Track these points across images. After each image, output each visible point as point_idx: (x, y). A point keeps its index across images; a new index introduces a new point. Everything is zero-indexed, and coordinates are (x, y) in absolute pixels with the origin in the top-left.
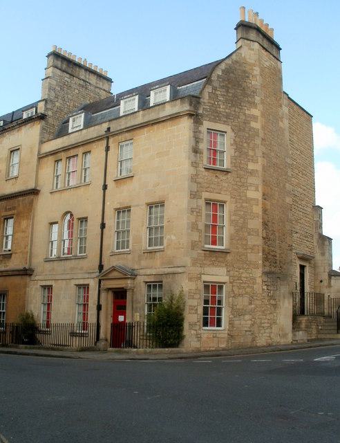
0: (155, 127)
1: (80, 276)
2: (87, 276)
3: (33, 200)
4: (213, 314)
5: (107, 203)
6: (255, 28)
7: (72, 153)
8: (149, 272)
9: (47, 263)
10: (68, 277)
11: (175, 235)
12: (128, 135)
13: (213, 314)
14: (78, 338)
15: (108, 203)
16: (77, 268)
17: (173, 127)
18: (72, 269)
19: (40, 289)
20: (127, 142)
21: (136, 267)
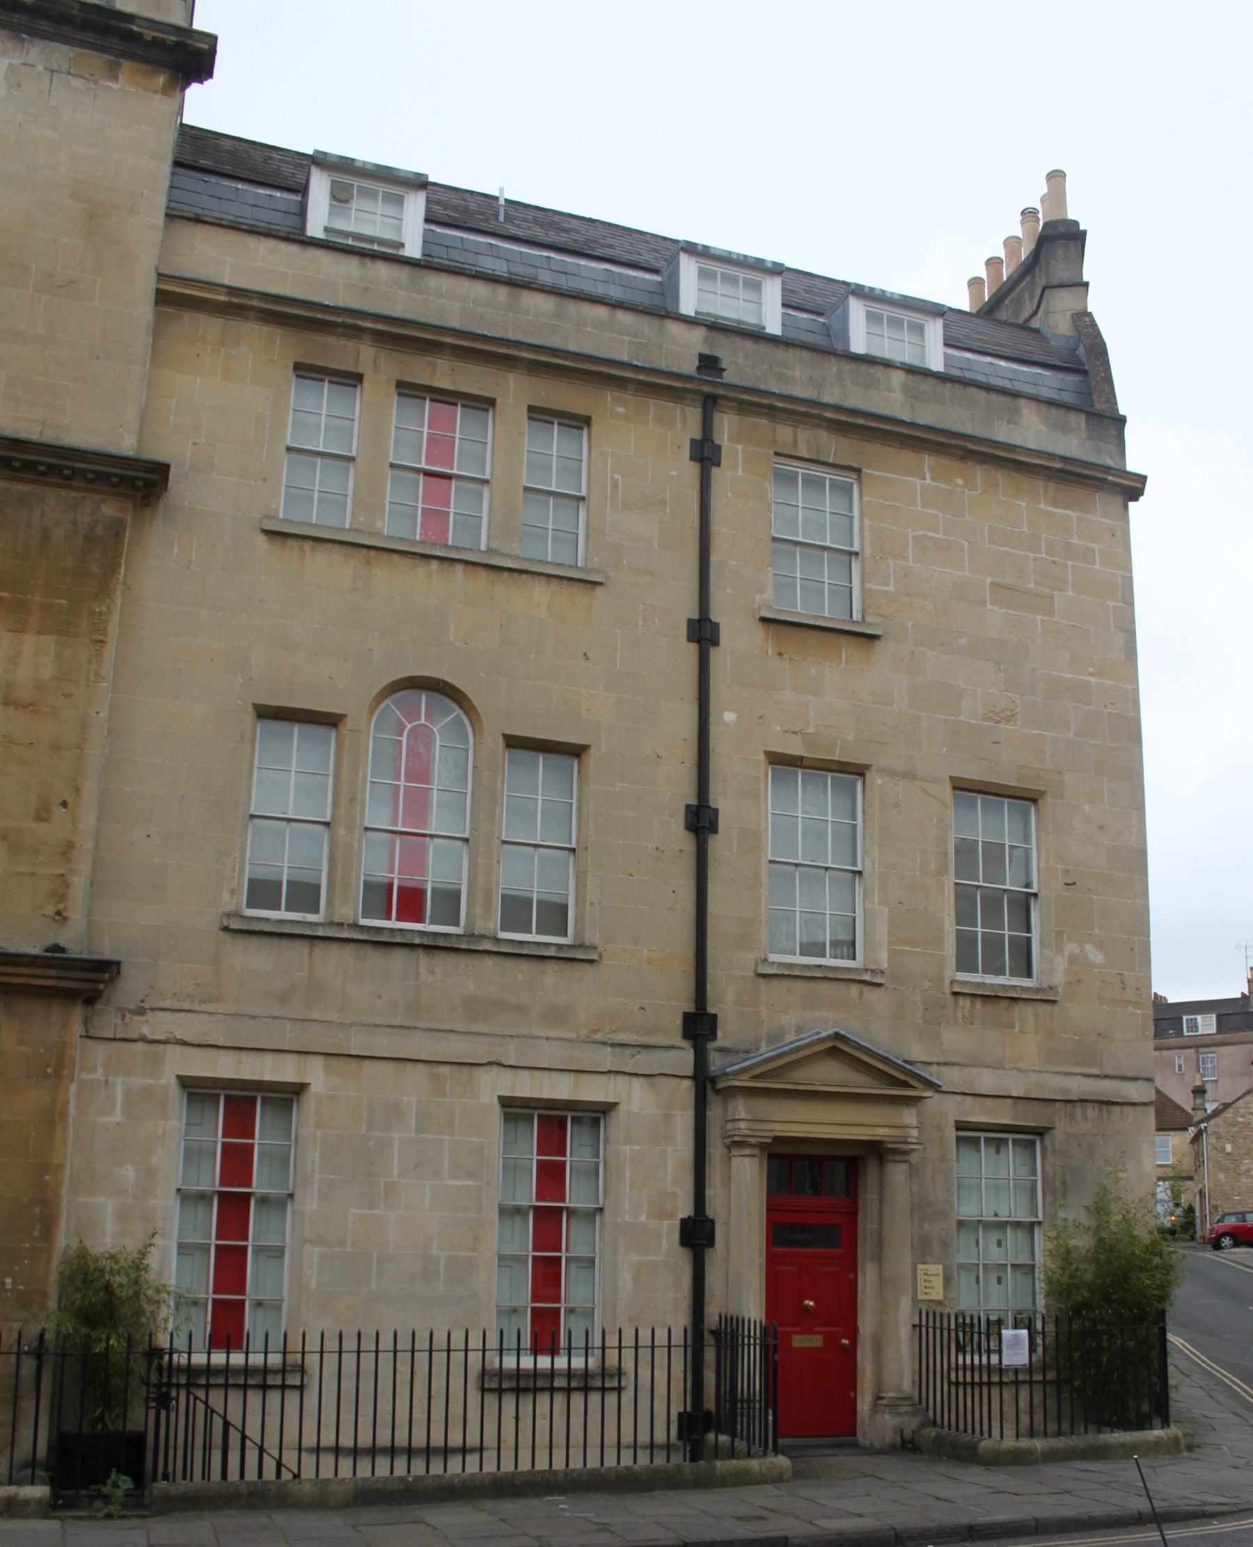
0: (979, 473)
1: (549, 1054)
2: (606, 1059)
3: (116, 531)
4: (993, 944)
5: (726, 717)
6: (839, 355)
7: (339, 351)
8: (987, 1081)
9: (241, 943)
10: (456, 1048)
11: (1100, 945)
12: (834, 446)
13: (993, 944)
14: (543, 1401)
15: (729, 717)
16: (522, 1010)
17: (349, 343)
18: (475, 1007)
19: (176, 1099)
20: (816, 471)
21: (916, 1052)
